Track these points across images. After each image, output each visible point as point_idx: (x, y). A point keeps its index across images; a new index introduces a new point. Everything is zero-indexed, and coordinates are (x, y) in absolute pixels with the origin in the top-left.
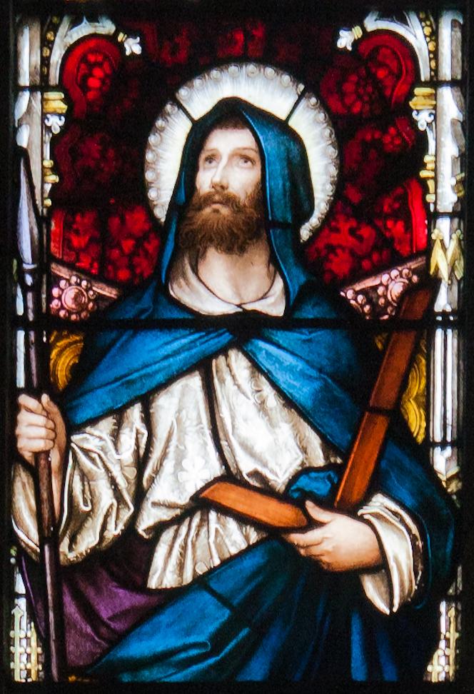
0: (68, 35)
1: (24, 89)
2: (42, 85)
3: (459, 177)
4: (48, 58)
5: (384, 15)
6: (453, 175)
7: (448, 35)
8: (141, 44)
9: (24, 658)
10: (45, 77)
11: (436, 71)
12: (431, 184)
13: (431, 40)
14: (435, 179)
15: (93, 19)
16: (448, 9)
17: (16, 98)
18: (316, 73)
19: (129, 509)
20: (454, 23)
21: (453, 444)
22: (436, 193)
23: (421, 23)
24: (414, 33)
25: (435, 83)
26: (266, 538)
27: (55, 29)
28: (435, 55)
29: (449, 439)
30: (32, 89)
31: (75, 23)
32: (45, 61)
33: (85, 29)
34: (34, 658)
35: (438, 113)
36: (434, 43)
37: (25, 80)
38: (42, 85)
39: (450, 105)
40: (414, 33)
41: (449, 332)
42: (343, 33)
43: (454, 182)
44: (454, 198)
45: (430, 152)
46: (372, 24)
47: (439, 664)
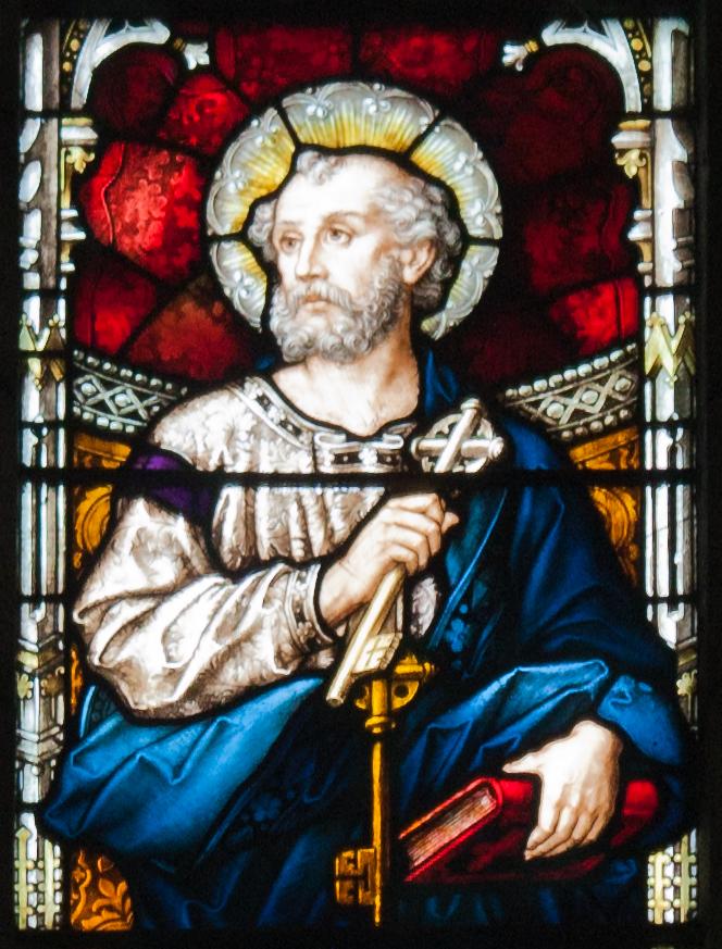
0: (99, 47)
1: (34, 115)
2: (59, 109)
3: (687, 263)
4: (71, 74)
5: (572, 22)
6: (676, 238)
7: (663, 51)
8: (209, 52)
9: (670, 893)
10: (66, 97)
11: (648, 97)
12: (646, 249)
13: (634, 37)
14: (651, 241)
15: (138, 22)
16: (666, 16)
17: (22, 126)
18: (464, 99)
19: (173, 692)
20: (676, 34)
21: (685, 599)
22: (653, 261)
23: (629, 41)
24: (613, 46)
25: (649, 111)
26: (490, 791)
27: (82, 36)
28: (646, 78)
29: (680, 590)
30: (47, 114)
31: (114, 28)
32: (67, 79)
33: (132, 35)
34: (684, 892)
35: (657, 270)
36: (646, 62)
37: (35, 101)
38: (59, 109)
39: (672, 149)
40: (613, 46)
41: (680, 489)
42: (508, 49)
43: (673, 245)
44: (678, 266)
45: (645, 259)
46: (553, 35)
47: (664, 899)
